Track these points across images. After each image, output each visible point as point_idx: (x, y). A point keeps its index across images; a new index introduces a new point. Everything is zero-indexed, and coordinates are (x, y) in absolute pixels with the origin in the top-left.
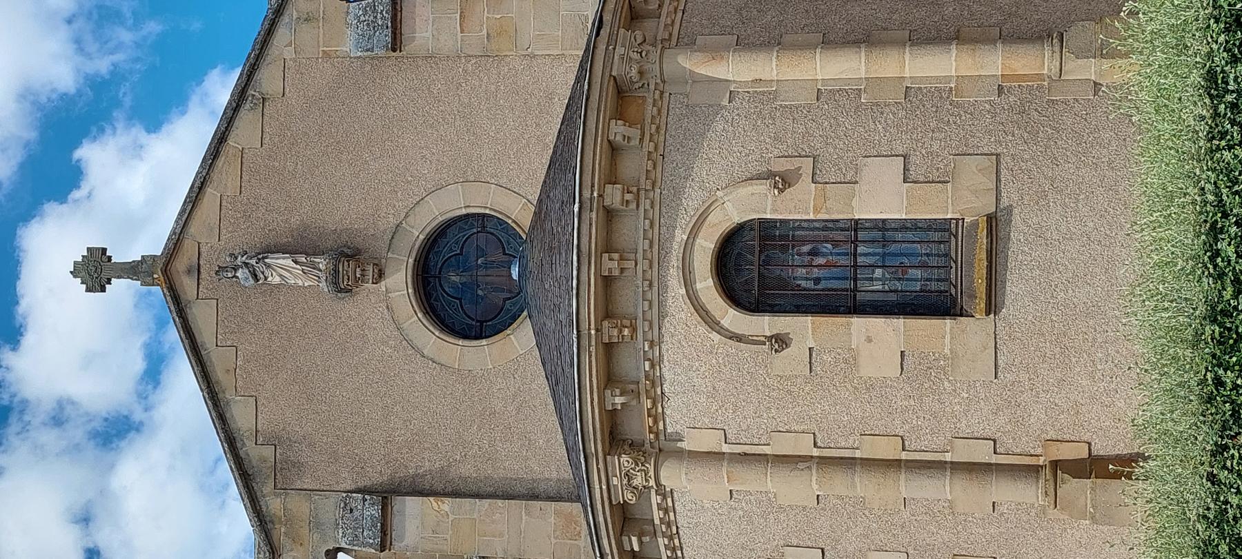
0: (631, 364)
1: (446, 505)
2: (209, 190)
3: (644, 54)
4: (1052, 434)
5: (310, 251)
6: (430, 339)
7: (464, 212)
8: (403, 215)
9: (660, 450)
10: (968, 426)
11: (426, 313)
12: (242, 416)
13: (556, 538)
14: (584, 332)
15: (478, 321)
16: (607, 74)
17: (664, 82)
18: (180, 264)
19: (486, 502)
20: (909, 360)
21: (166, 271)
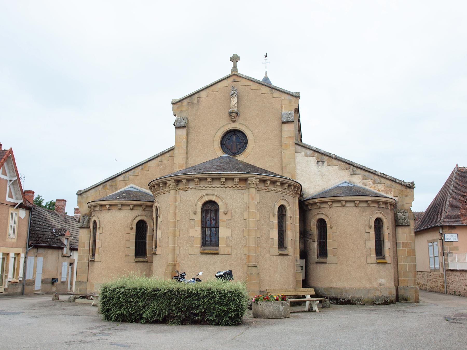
0: (191, 185)
1: (185, 140)
2: (252, 82)
3: (254, 184)
4: (180, 265)
5: (239, 106)
7: (248, 139)
8: (247, 126)
9: (177, 190)
10: (181, 249)
11: (226, 132)
12: (203, 94)
13: (178, 164)
14: (196, 175)
15: (225, 143)
16: (248, 177)
17: (249, 188)
19: (185, 148)
20: (193, 238)
21: (234, 75)
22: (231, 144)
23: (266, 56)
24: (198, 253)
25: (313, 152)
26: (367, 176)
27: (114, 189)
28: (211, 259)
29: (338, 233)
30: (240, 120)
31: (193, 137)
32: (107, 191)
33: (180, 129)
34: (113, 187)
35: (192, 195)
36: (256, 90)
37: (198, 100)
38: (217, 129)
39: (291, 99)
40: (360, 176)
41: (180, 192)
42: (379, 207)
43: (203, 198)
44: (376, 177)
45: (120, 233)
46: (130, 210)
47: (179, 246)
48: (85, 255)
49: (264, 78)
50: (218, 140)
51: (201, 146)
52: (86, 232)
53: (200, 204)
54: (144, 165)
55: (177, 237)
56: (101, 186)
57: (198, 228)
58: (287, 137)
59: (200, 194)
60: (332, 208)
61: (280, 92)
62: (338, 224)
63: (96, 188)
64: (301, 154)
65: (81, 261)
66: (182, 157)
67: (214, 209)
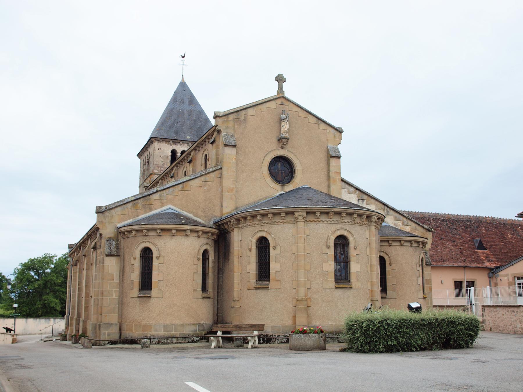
2: (300, 109)
6: (269, 159)
12: (250, 111)
18: (283, 100)
20: (326, 272)
22: (276, 171)
23: (183, 57)
24: (333, 288)
25: (355, 189)
26: (397, 217)
27: (147, 209)
28: (345, 293)
29: (397, 270)
30: (289, 147)
31: (240, 159)
32: (138, 210)
33: (229, 148)
34: (147, 206)
35: (324, 228)
36: (304, 118)
37: (245, 117)
38: (266, 154)
39: (335, 133)
40: (392, 217)
41: (309, 224)
42: (411, 246)
43: (336, 232)
44: (405, 219)
45: (187, 264)
46: (197, 238)
47: (310, 280)
48: (114, 290)
49: (181, 82)
50: (267, 165)
51: (249, 169)
52: (115, 261)
53: (333, 238)
54: (184, 183)
55: (307, 271)
56: (131, 204)
57: (332, 262)
58: (334, 172)
59: (333, 228)
60: (391, 246)
61: (326, 125)
62: (397, 262)
63: (124, 206)
64: (344, 190)
65: (108, 298)
66: (232, 180)
67: (342, 244)
